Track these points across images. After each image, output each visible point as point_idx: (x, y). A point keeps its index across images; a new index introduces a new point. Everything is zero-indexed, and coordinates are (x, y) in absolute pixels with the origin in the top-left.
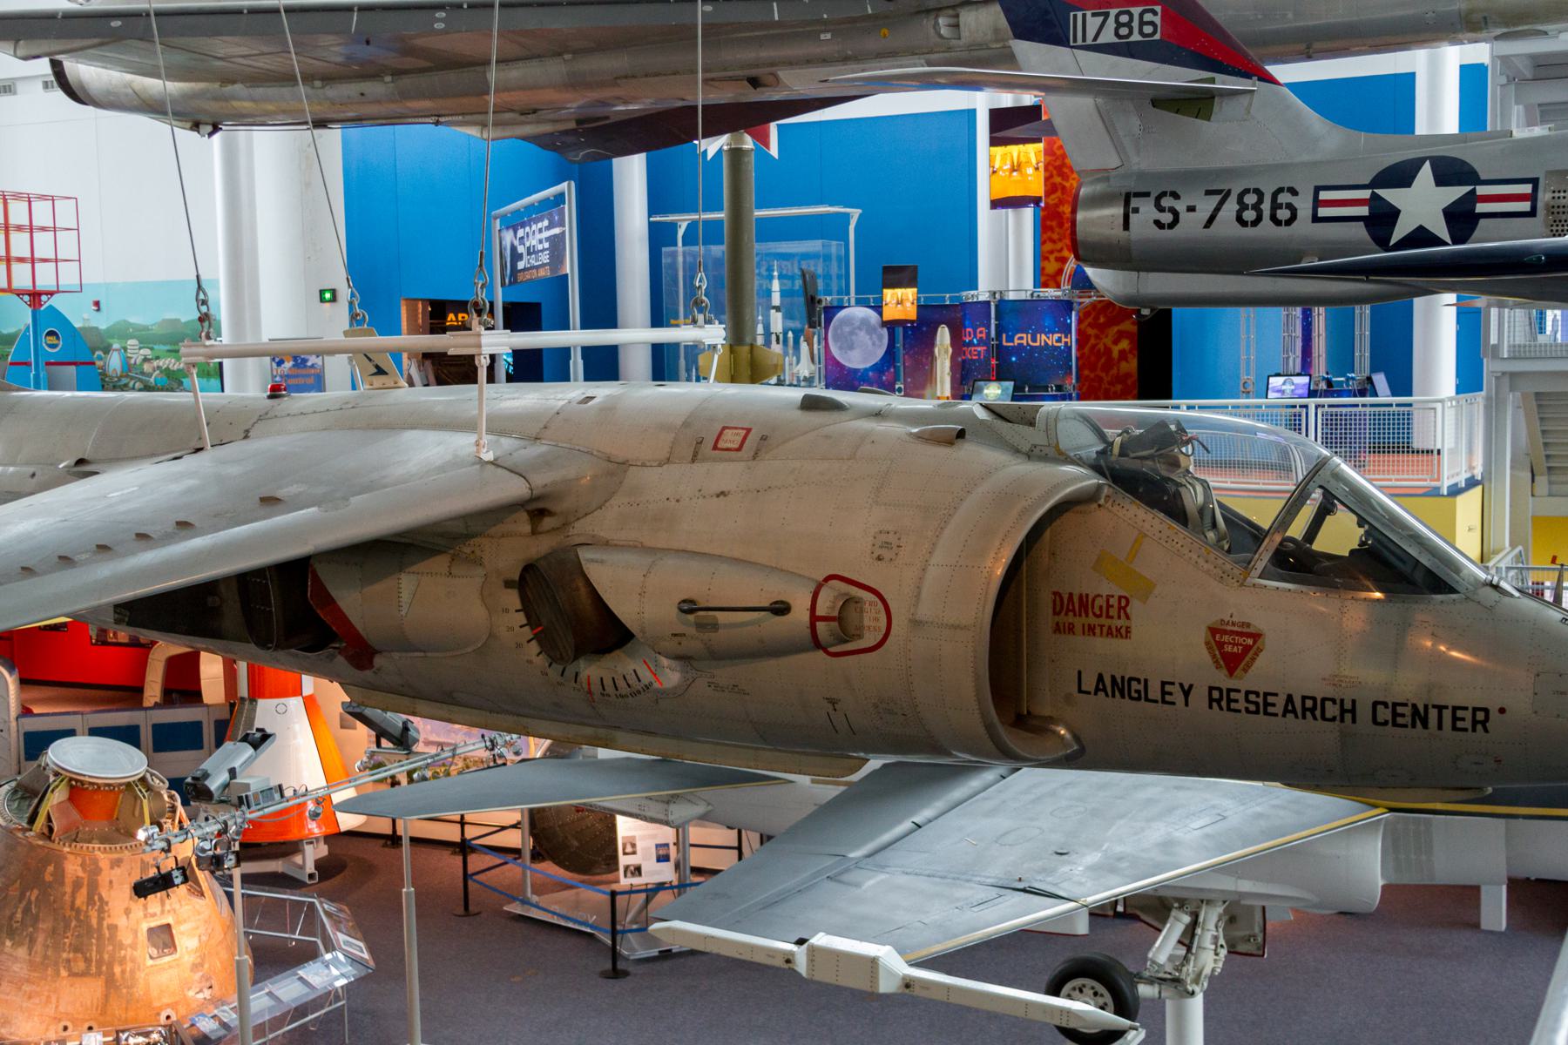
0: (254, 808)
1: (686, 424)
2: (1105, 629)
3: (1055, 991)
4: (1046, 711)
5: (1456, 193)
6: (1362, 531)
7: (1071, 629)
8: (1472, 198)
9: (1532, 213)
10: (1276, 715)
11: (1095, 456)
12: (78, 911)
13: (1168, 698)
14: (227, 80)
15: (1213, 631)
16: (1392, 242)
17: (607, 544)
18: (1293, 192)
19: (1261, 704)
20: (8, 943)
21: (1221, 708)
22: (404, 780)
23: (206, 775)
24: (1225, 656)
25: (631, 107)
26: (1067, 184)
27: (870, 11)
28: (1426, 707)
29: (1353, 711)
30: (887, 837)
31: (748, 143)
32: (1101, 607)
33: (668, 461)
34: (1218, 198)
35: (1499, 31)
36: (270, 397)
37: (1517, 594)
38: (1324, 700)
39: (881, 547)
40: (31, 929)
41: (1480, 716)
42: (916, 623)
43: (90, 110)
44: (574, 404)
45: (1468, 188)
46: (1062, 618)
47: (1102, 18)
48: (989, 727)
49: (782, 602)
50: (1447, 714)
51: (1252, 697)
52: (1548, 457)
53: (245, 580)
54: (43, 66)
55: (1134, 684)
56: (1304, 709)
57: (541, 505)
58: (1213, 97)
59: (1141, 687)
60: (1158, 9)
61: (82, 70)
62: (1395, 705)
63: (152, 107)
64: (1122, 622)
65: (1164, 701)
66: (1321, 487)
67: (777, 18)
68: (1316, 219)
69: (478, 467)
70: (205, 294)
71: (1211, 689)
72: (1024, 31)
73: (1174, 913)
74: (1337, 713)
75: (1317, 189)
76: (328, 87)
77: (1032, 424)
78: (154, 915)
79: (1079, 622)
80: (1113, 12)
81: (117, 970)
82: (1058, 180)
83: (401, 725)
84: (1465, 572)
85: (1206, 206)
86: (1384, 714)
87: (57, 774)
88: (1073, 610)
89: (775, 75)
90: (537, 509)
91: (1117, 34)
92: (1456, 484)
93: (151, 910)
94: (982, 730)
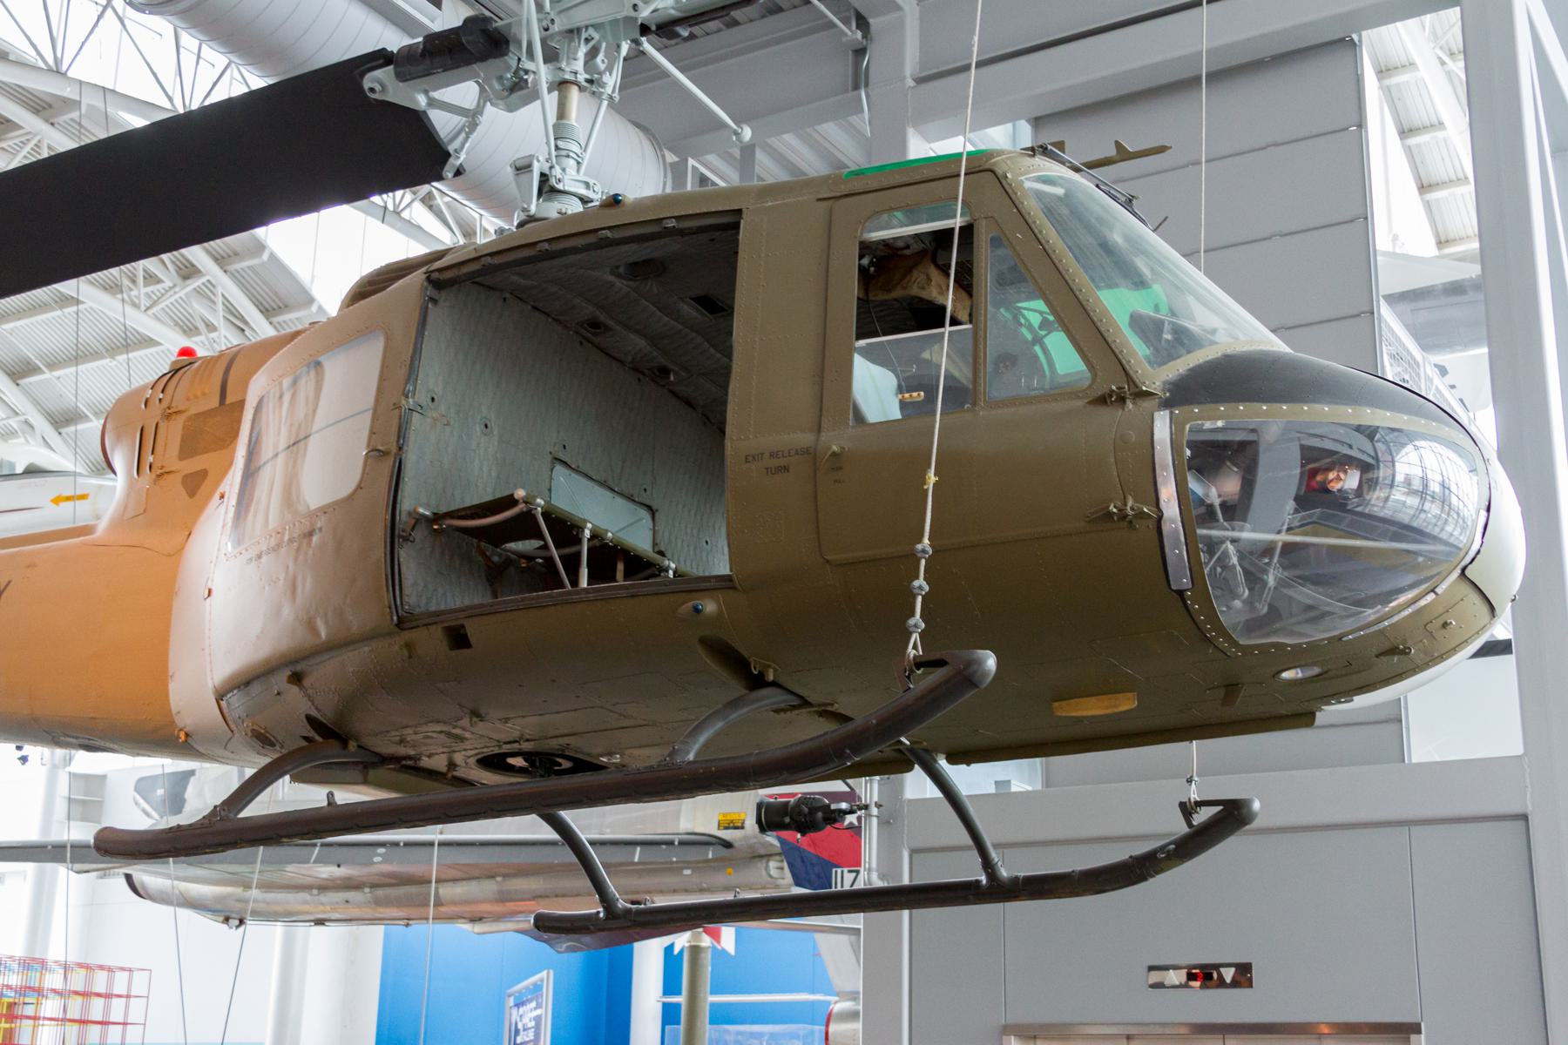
31: (706, 941)
43: (147, 903)
47: (854, 874)
76: (322, 895)
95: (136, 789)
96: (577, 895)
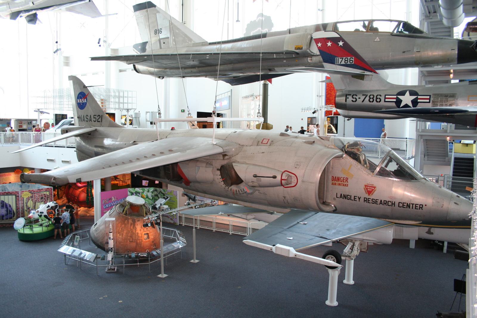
0: (165, 212)
1: (256, 138)
2: (343, 185)
3: (324, 258)
4: (329, 201)
5: (414, 97)
6: (397, 166)
7: (335, 184)
8: (417, 99)
9: (429, 102)
10: (378, 204)
11: (342, 148)
12: (131, 230)
13: (355, 200)
14: (166, 68)
15: (366, 186)
16: (401, 107)
17: (238, 162)
18: (380, 96)
19: (375, 202)
20: (118, 235)
21: (366, 202)
22: (194, 208)
23: (156, 205)
24: (368, 191)
25: (245, 74)
26: (332, 93)
27: (294, 56)
28: (410, 204)
29: (394, 204)
30: (292, 225)
32: (342, 180)
33: (252, 145)
34: (365, 96)
35: (422, 66)
36: (172, 130)
37: (429, 181)
38: (388, 201)
39: (296, 165)
40: (122, 232)
41: (421, 206)
42: (303, 181)
44: (233, 133)
45: (416, 97)
46: (334, 182)
47: (342, 59)
48: (317, 204)
49: (275, 176)
50: (414, 206)
51: (373, 200)
52: (428, 152)
53: (165, 167)
54: (131, 66)
55: (348, 196)
56: (384, 203)
57: (225, 154)
58: (364, 76)
59: (350, 197)
60: (353, 58)
61: (139, 67)
62: (403, 203)
63: (151, 73)
64: (346, 183)
65: (354, 200)
66: (389, 156)
67: (275, 57)
68: (385, 101)
69: (212, 145)
70: (160, 109)
71: (365, 198)
72: (326, 61)
73: (350, 243)
74: (391, 204)
75: (385, 95)
77: (329, 141)
78: (145, 231)
79: (337, 183)
80: (344, 58)
81: (138, 241)
82: (330, 92)
83: (194, 197)
84: (419, 176)
85: (362, 98)
86: (401, 205)
87: (128, 203)
88: (336, 180)
89: (274, 69)
90: (224, 155)
91: (345, 62)
92: (409, 157)
93: (145, 230)
94: (316, 204)
95: (133, 47)
96: (250, 68)
